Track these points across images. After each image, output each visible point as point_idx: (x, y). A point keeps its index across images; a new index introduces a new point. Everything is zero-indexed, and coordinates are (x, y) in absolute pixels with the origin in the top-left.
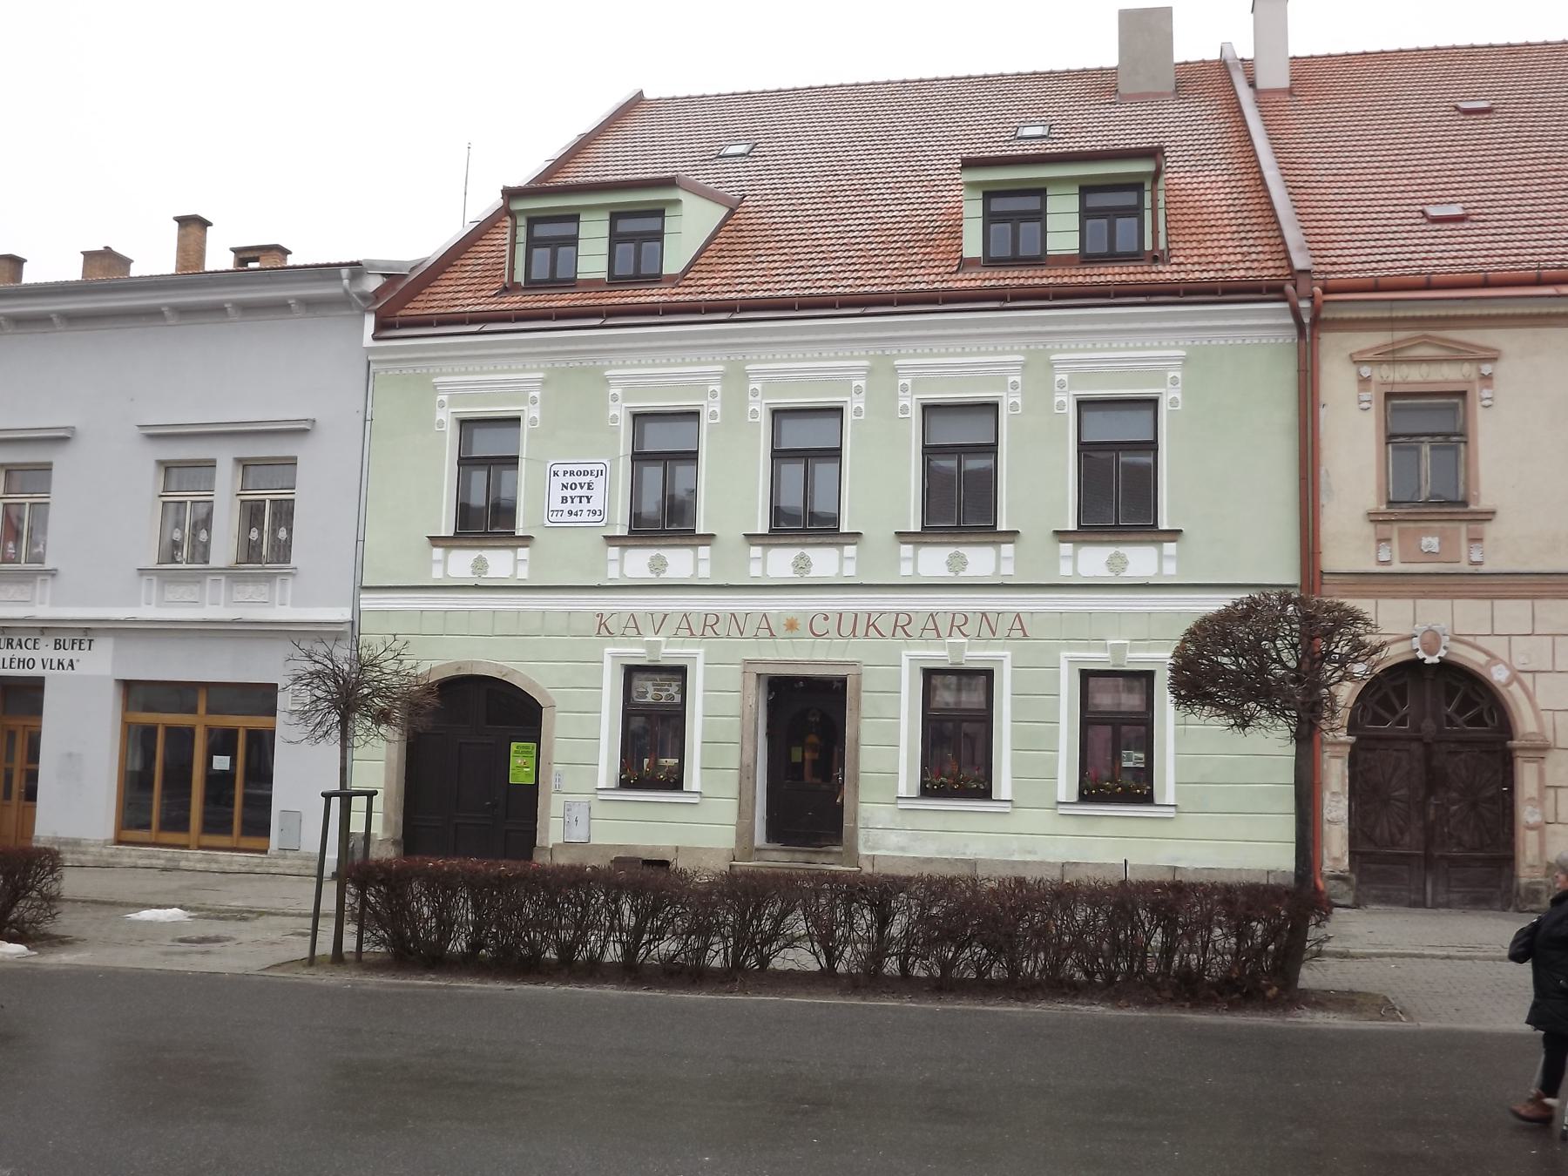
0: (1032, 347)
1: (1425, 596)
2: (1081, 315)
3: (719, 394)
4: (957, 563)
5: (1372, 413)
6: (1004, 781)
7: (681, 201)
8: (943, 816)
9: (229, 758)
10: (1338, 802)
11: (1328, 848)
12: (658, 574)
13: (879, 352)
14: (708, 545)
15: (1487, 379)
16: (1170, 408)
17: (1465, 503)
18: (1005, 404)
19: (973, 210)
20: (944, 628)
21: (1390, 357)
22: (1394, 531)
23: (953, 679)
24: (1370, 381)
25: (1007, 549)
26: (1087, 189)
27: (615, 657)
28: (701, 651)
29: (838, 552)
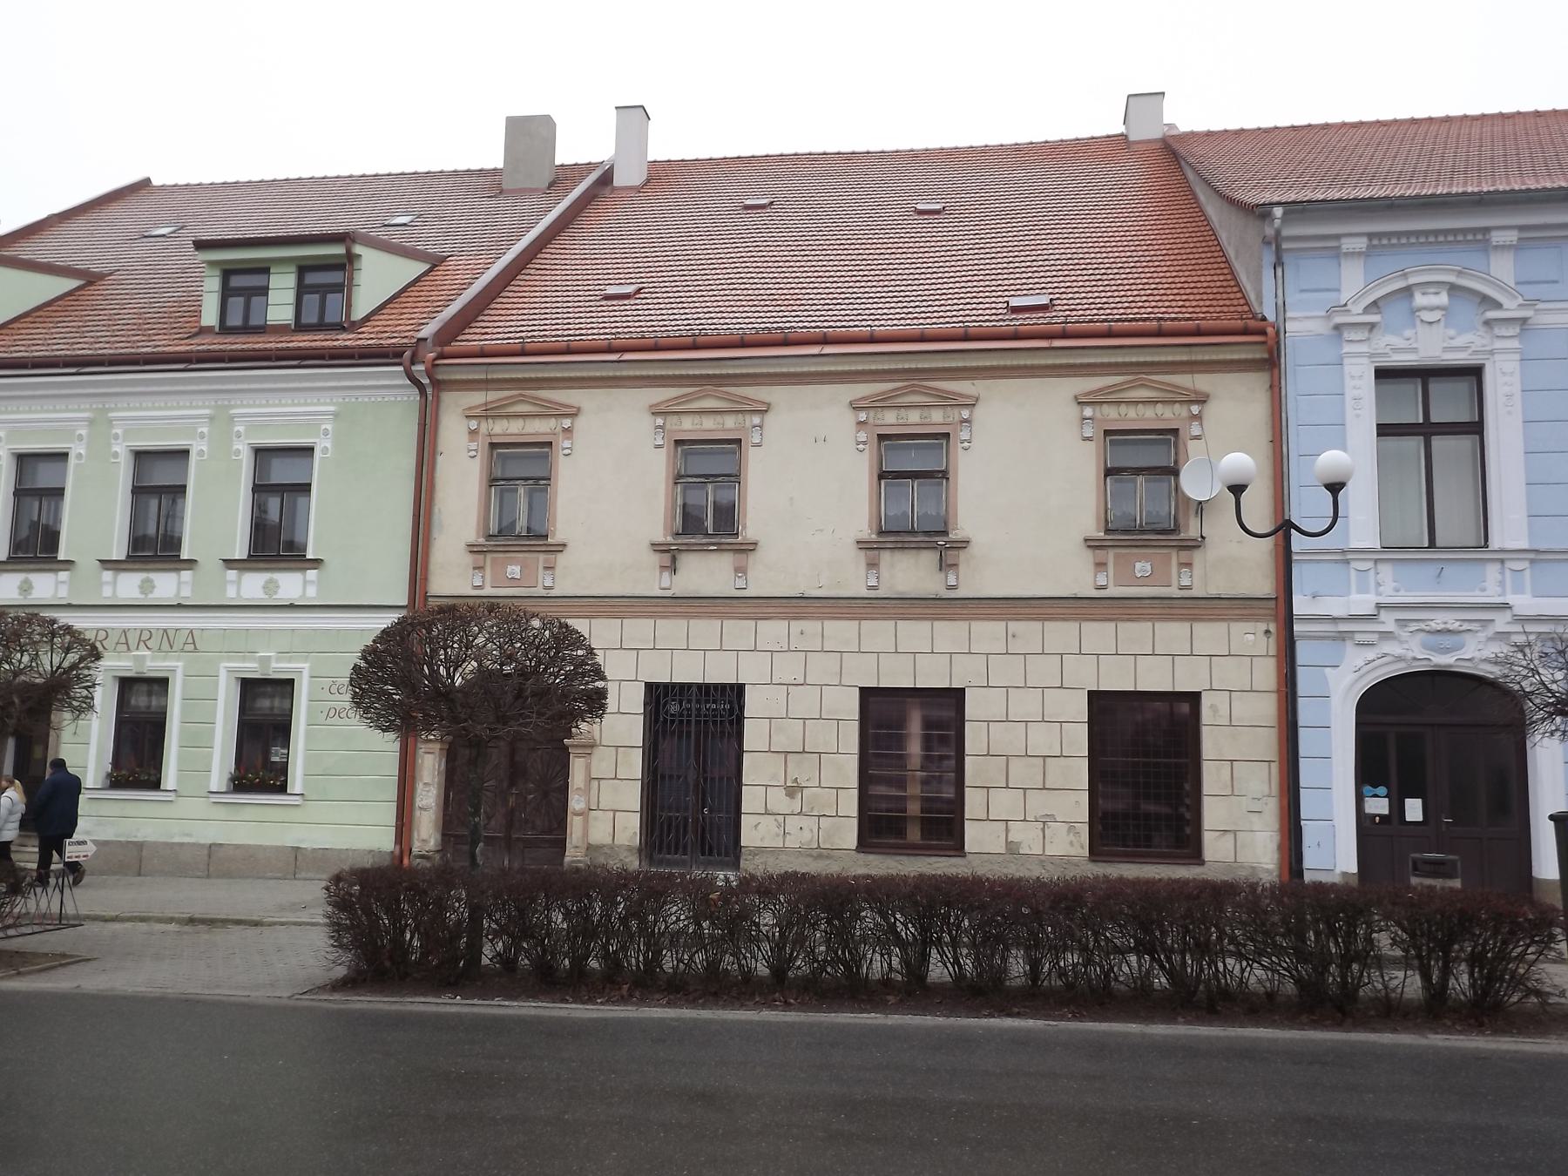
0: (219, 403)
1: (698, 616)
2: (124, 380)
3: (331, 432)
4: (147, 587)
5: (478, 459)
6: (170, 777)
7: (360, 255)
8: (121, 804)
9: (1420, 800)
10: (428, 791)
11: (418, 831)
12: (271, 596)
13: (100, 406)
14: (315, 569)
15: (568, 431)
16: (321, 455)
17: (945, 533)
18: (194, 451)
19: (212, 284)
20: (133, 641)
21: (489, 413)
22: (1110, 555)
23: (144, 688)
24: (477, 433)
25: (186, 575)
26: (304, 268)
27: (229, 671)
28: (306, 665)
29: (302, 577)
